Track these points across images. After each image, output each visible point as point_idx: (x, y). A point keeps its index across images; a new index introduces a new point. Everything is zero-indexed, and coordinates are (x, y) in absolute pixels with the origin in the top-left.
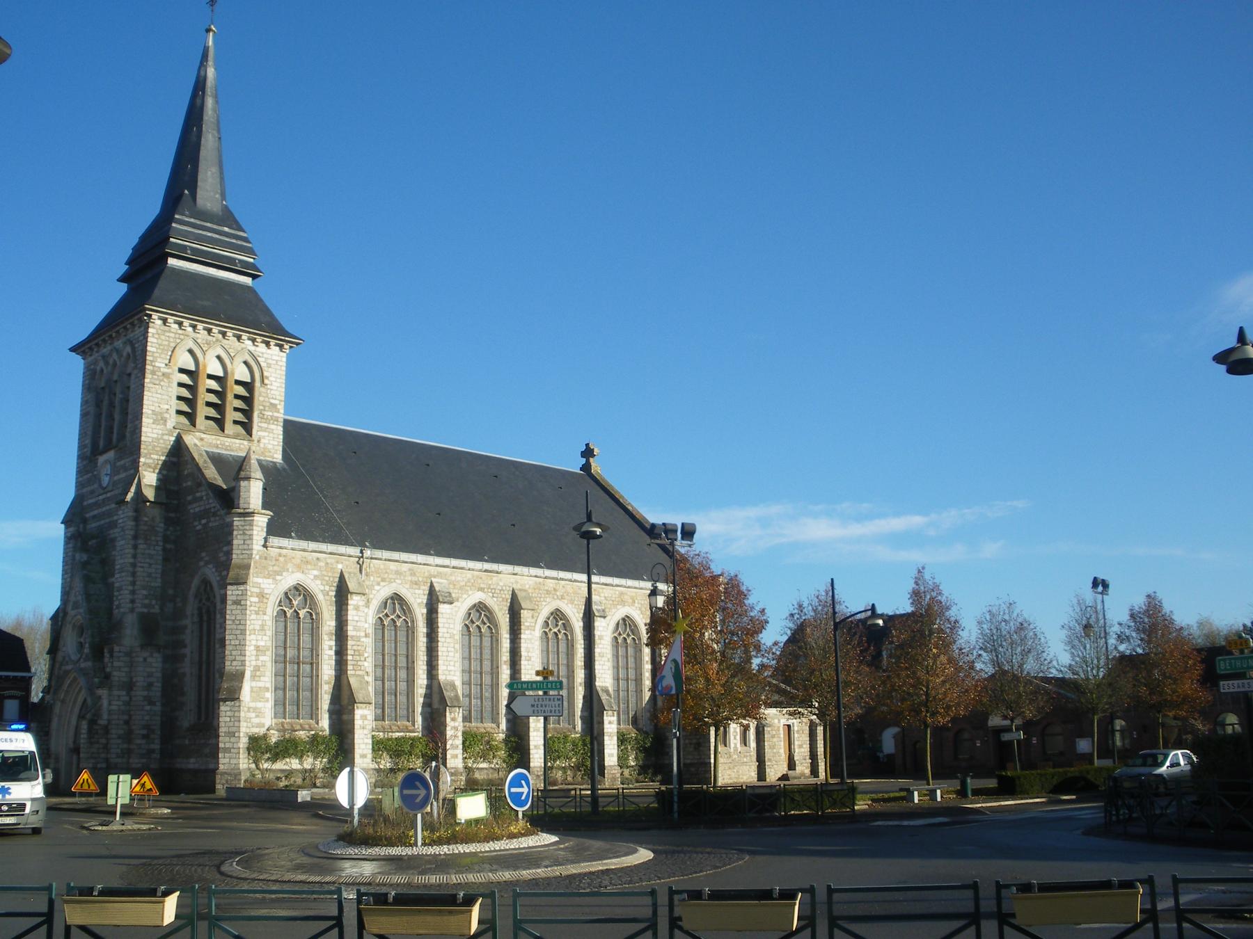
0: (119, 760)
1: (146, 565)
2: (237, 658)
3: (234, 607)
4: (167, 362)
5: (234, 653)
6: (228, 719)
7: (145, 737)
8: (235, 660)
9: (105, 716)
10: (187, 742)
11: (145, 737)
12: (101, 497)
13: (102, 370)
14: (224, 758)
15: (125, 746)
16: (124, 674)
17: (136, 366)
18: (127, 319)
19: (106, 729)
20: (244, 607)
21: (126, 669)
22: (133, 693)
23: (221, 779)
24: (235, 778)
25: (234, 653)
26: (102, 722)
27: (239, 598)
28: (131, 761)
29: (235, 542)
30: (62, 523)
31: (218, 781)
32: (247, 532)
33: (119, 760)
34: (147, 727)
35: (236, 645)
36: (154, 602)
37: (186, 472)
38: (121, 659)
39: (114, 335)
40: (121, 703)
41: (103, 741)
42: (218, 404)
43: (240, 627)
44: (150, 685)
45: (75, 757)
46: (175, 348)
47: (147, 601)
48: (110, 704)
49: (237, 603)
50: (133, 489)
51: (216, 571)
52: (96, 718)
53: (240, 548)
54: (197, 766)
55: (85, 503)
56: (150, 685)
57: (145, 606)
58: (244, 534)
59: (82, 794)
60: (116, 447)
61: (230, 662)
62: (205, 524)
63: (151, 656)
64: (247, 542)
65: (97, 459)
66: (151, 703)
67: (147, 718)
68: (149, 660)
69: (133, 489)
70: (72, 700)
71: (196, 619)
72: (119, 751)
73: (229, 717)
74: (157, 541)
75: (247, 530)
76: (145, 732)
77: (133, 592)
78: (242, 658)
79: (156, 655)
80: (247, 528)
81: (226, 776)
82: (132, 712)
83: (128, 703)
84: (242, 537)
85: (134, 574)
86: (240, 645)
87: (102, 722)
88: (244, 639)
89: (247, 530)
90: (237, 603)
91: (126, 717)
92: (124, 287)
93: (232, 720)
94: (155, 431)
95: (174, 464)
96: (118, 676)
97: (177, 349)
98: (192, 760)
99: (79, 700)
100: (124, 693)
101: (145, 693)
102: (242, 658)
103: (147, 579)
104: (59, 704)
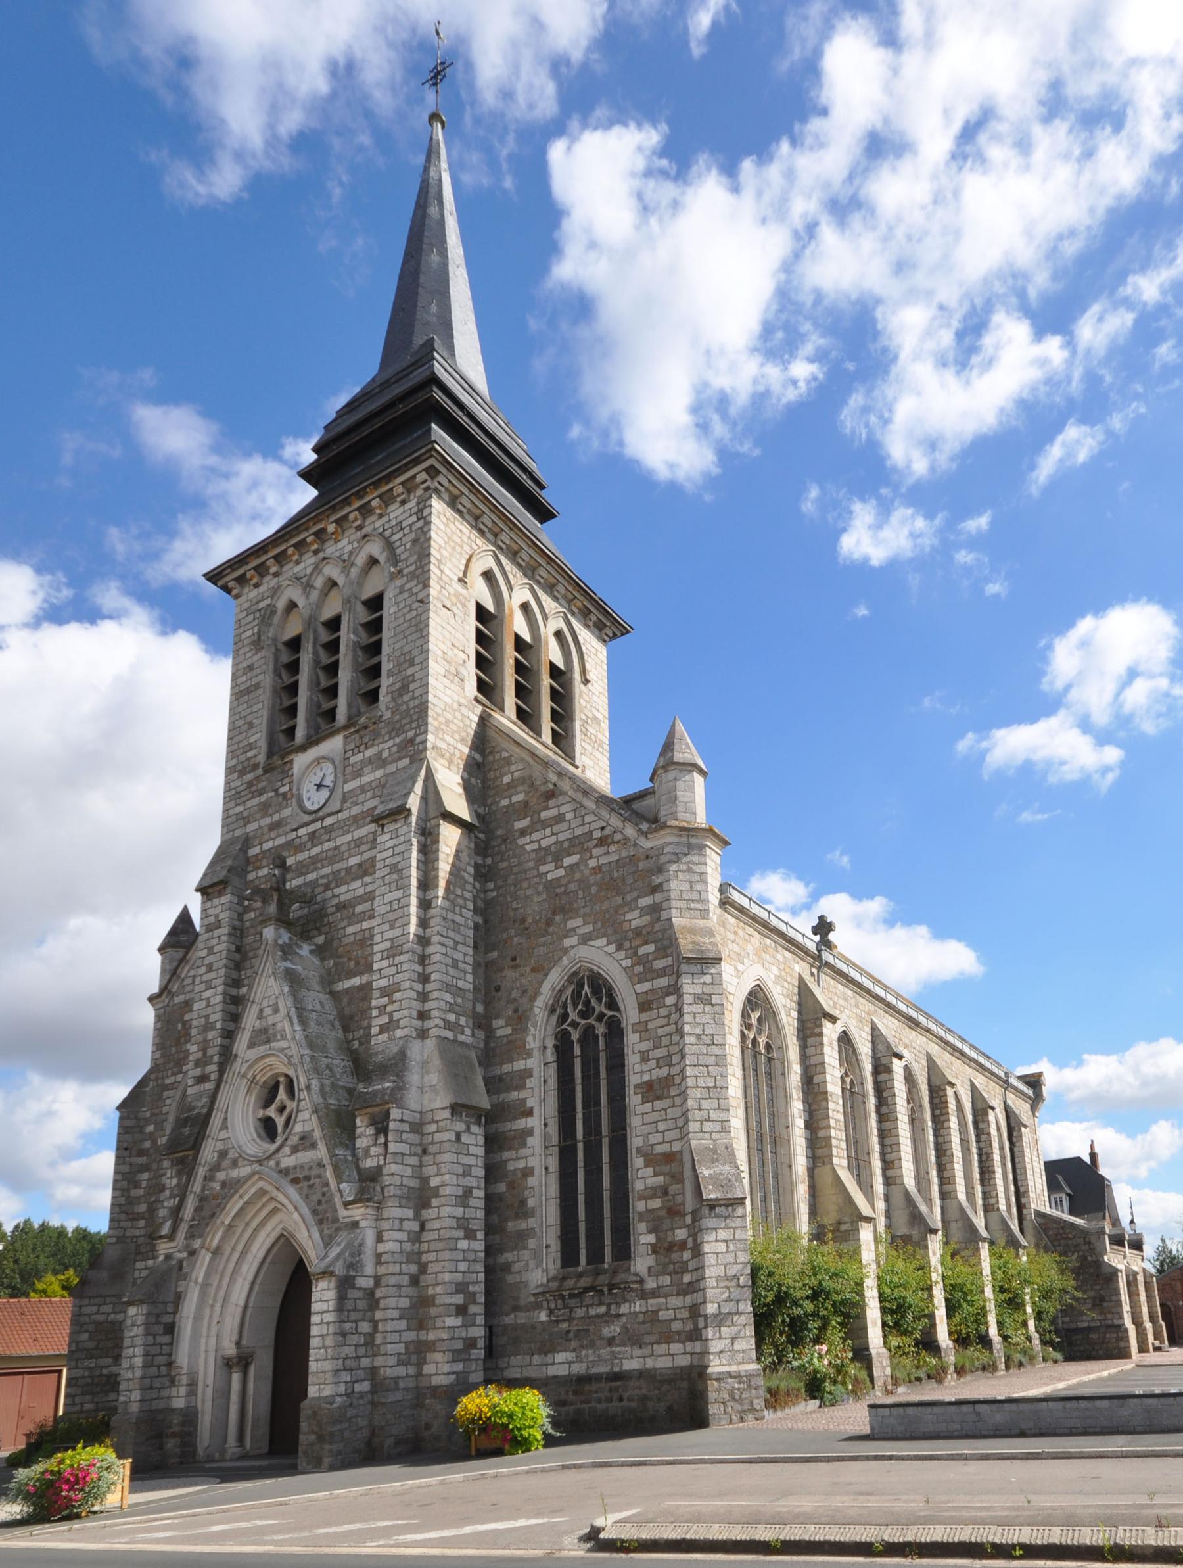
0: (401, 1371)
1: (450, 943)
2: (713, 1115)
3: (698, 1008)
4: (461, 575)
5: (705, 1104)
6: (722, 1247)
7: (461, 1310)
8: (708, 1120)
9: (369, 1269)
10: (543, 1316)
11: (461, 1310)
12: (302, 832)
13: (292, 605)
14: (720, 1338)
15: (411, 1336)
16: (409, 1171)
17: (400, 571)
18: (376, 484)
19: (372, 1301)
20: (717, 1008)
21: (414, 1161)
22: (429, 1213)
23: (719, 1390)
24: (749, 1386)
25: (705, 1104)
26: (364, 1282)
27: (707, 990)
28: (428, 1369)
29: (673, 885)
30: (197, 890)
31: (712, 1396)
32: (695, 867)
33: (401, 1371)
34: (461, 1288)
35: (708, 1088)
36: (463, 1021)
37: (507, 779)
38: (405, 1136)
39: (331, 528)
40: (403, 1236)
41: (365, 1327)
42: (194, 928)
43: (715, 1050)
44: (468, 1192)
45: (236, 1377)
46: (471, 557)
47: (452, 1017)
48: (379, 1239)
49: (704, 999)
50: (418, 788)
51: (619, 948)
52: (352, 1273)
53: (685, 896)
54: (578, 1369)
55: (252, 852)
56: (468, 1192)
57: (448, 1025)
58: (690, 870)
59: (231, 1460)
60: (345, 727)
61: (698, 1125)
62: (572, 867)
63: (468, 1130)
64: (698, 887)
65: (291, 761)
66: (470, 1235)
67: (463, 1266)
68: (465, 1138)
69: (418, 788)
70: (240, 1247)
71: (550, 1056)
72: (401, 1348)
73: (726, 1241)
74: (465, 899)
75: (694, 863)
76: (459, 1299)
77: (423, 997)
78: (722, 1115)
79: (475, 1129)
80: (695, 858)
81: (730, 1380)
82: (424, 1258)
83: (416, 1237)
84: (687, 876)
85: (423, 959)
86: (715, 1087)
87: (364, 1282)
88: (724, 1076)
89: (694, 863)
90: (704, 999)
91: (413, 1269)
92: (308, 494)
93: (731, 1247)
94: (448, 692)
95: (479, 765)
96: (396, 1175)
97: (474, 560)
98: (560, 1357)
99: (254, 1248)
100: (410, 1213)
101: (459, 1212)
102: (722, 1115)
103: (451, 971)
104: (205, 1258)
